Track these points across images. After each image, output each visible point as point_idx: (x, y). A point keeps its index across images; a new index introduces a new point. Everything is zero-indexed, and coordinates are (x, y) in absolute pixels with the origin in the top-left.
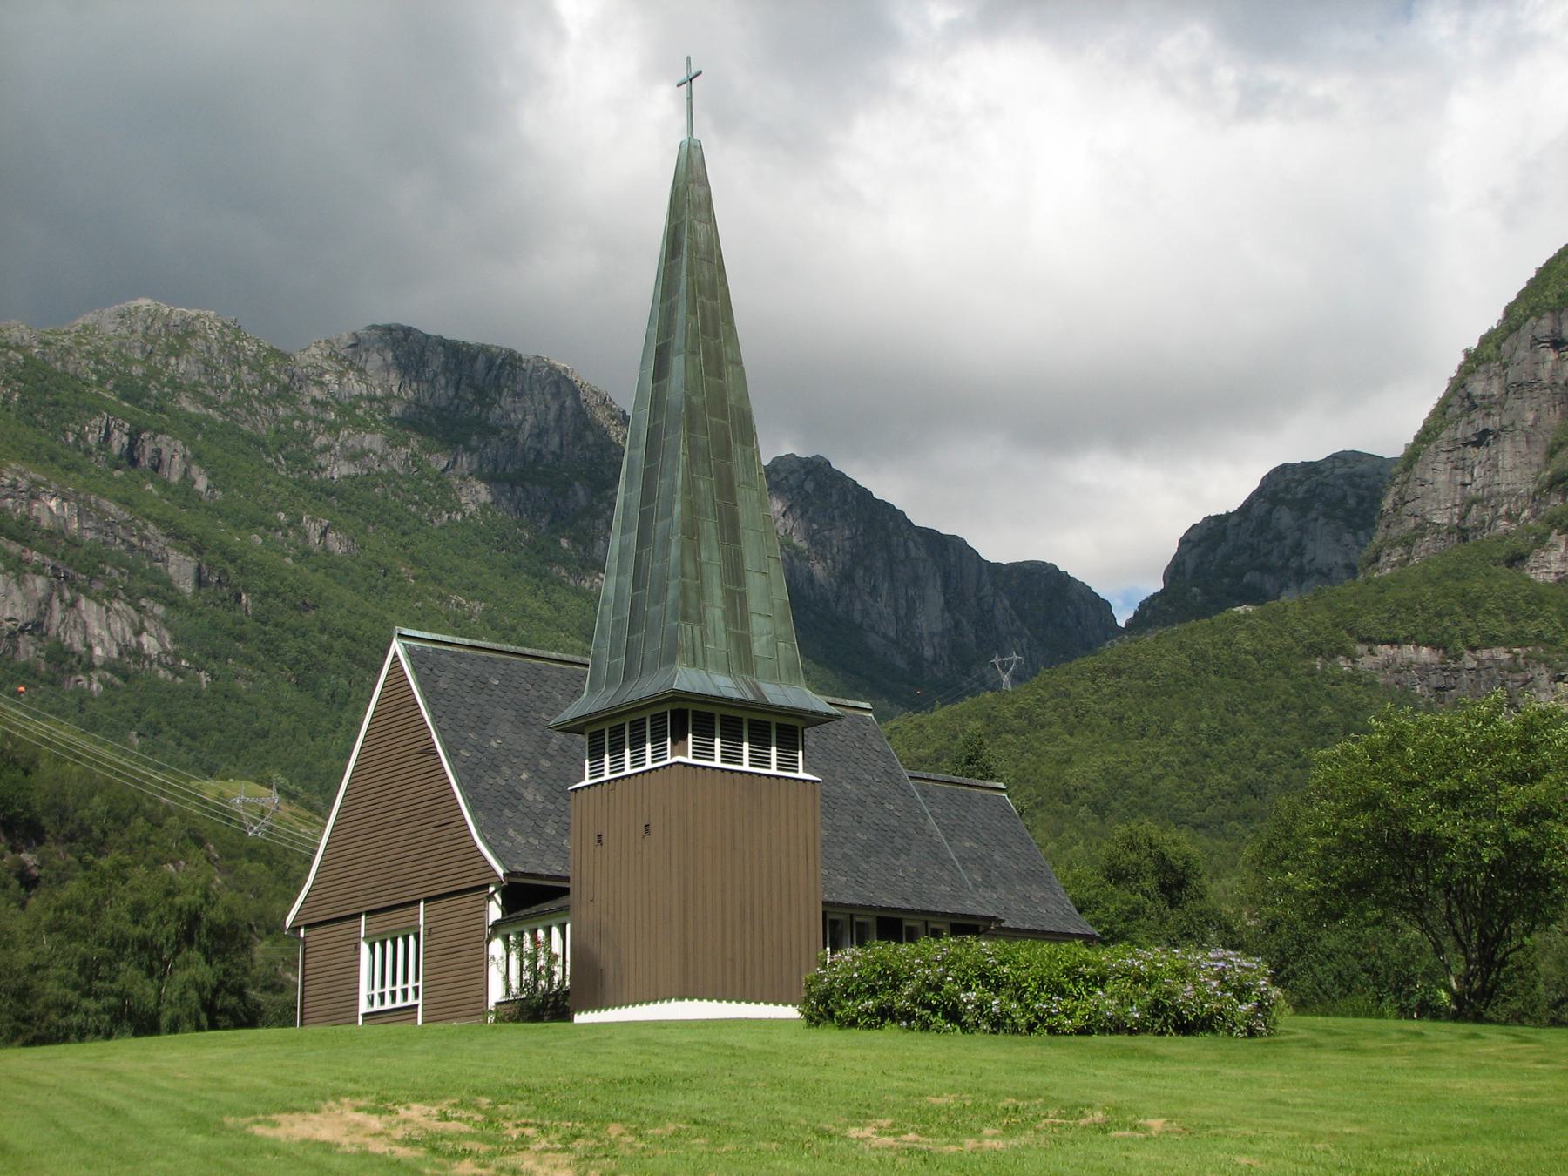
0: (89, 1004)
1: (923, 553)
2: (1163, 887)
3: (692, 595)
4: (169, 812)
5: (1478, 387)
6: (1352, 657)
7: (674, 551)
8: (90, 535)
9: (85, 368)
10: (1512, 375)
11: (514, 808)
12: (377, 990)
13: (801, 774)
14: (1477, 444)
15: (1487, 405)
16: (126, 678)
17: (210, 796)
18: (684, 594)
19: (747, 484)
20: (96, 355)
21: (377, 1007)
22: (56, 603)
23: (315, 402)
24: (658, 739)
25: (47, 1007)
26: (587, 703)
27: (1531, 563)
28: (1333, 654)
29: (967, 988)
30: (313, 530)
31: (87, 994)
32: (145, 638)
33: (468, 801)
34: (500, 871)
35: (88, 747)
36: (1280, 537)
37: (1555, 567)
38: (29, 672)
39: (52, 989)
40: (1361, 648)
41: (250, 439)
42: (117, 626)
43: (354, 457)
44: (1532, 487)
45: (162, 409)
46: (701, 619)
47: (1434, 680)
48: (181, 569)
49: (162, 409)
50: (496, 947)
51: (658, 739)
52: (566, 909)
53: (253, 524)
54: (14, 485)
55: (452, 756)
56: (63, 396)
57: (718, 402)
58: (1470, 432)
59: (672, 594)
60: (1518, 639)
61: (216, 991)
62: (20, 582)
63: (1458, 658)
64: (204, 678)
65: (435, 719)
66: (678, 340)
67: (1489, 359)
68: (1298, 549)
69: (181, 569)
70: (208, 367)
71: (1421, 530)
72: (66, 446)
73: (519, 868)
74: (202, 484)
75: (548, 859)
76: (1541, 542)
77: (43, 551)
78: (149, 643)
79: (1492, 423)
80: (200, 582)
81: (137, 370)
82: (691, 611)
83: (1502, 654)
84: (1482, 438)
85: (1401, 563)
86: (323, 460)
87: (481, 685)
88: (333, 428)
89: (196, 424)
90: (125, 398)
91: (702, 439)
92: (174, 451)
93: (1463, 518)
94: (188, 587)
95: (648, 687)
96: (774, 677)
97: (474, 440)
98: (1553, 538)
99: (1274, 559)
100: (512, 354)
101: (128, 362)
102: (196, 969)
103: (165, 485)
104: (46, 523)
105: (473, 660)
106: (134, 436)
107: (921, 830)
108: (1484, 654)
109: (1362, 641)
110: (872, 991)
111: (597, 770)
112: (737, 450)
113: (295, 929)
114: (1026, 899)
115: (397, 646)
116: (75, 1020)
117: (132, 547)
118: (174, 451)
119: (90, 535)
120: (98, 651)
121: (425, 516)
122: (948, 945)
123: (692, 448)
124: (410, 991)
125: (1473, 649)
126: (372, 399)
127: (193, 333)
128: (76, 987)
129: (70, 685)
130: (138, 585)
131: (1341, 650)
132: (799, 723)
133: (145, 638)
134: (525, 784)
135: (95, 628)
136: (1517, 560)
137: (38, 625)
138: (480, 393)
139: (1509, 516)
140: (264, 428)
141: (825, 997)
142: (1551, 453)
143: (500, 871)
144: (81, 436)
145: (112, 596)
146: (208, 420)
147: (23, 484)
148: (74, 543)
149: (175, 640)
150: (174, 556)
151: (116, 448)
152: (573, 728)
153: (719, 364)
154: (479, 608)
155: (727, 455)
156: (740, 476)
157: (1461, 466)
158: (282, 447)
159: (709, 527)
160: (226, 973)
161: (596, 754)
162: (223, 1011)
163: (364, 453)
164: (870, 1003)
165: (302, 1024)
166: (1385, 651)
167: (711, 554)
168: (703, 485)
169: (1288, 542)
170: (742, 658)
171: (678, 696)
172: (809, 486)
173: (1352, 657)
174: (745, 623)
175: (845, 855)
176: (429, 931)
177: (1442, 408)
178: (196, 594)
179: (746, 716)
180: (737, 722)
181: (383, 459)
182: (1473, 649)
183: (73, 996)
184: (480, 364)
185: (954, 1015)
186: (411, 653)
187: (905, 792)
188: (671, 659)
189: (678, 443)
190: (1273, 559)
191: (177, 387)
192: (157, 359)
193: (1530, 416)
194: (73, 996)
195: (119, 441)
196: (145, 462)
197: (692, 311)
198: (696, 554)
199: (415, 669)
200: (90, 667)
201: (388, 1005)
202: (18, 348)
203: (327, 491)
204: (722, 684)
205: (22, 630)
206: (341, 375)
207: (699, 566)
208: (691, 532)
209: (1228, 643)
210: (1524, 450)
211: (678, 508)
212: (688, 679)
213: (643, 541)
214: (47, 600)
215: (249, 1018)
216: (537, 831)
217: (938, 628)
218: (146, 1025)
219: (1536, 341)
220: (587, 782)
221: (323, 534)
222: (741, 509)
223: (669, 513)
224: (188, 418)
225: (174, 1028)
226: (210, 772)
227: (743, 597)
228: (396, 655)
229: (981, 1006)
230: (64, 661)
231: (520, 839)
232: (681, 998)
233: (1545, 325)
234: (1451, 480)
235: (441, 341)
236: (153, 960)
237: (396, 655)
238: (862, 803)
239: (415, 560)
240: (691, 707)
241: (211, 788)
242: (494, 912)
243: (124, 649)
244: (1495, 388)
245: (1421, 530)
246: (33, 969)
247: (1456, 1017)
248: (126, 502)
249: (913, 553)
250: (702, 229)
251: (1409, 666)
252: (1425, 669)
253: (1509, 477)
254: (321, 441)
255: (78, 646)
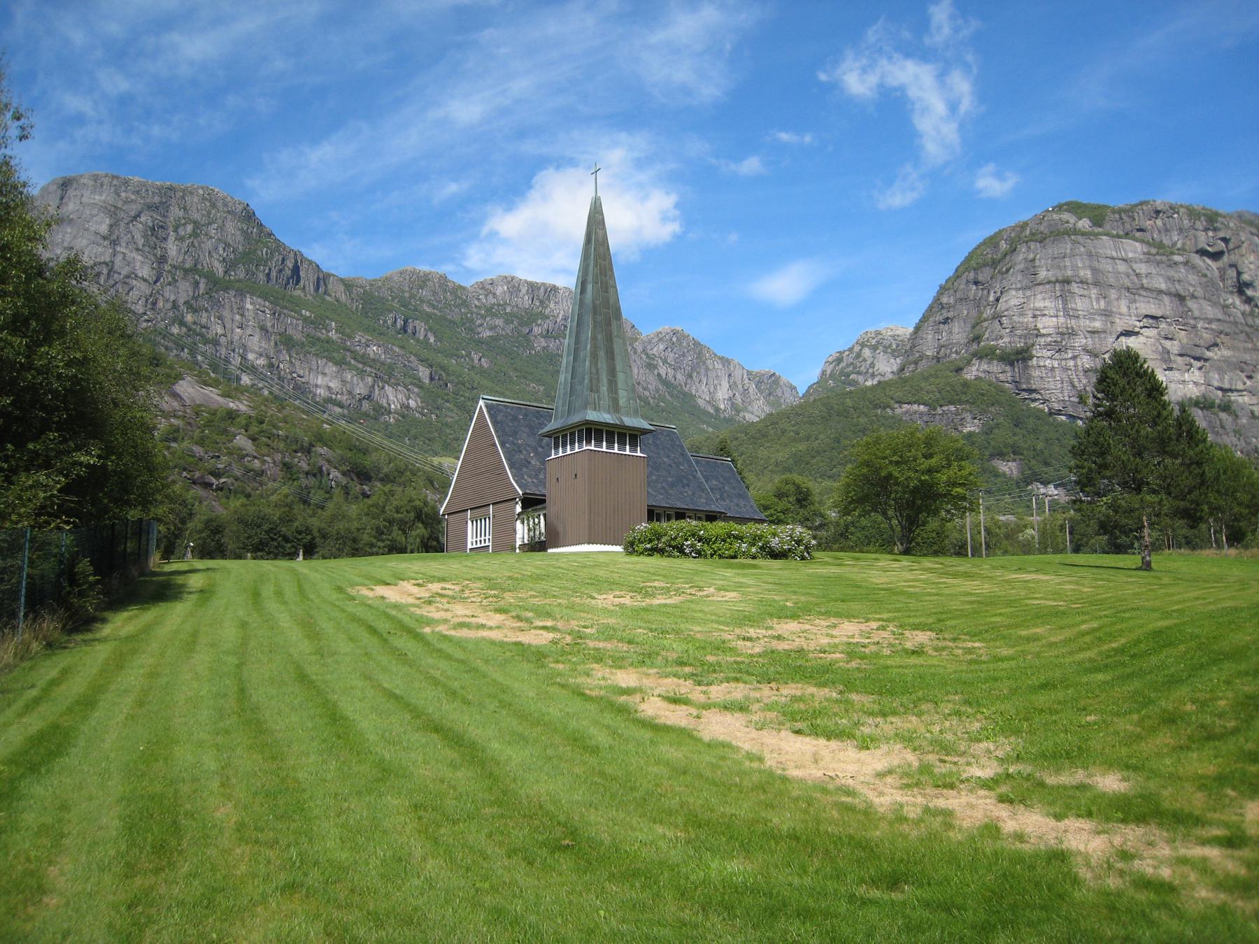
0: (381, 544)
1: (720, 366)
2: (798, 501)
3: (594, 382)
4: (419, 470)
5: (945, 300)
6: (893, 409)
7: (587, 363)
8: (389, 360)
9: (386, 294)
10: (959, 295)
11: (527, 467)
12: (483, 538)
13: (639, 454)
14: (944, 323)
15: (949, 307)
16: (403, 417)
17: (436, 463)
18: (591, 381)
19: (617, 336)
20: (391, 289)
21: (474, 546)
22: (376, 387)
23: (476, 306)
24: (580, 441)
25: (365, 545)
26: (552, 425)
27: (965, 371)
28: (884, 408)
29: (687, 540)
30: (476, 357)
31: (378, 540)
32: (410, 401)
33: (508, 464)
34: (521, 493)
35: (388, 444)
36: (865, 360)
37: (974, 373)
38: (366, 415)
39: (366, 538)
40: (897, 405)
41: (451, 321)
42: (400, 396)
43: (492, 328)
44: (966, 341)
45: (416, 310)
46: (598, 391)
47: (925, 418)
48: (424, 373)
49: (416, 310)
50: (518, 524)
51: (580, 441)
52: (544, 508)
53: (452, 356)
54: (360, 341)
55: (503, 445)
56: (379, 306)
57: (606, 303)
58: (941, 318)
59: (586, 381)
60: (960, 402)
61: (428, 539)
62: (362, 379)
63: (935, 409)
64: (433, 416)
65: (496, 432)
66: (590, 278)
67: (949, 289)
68: (872, 365)
69: (424, 373)
70: (434, 293)
71: (921, 357)
72: (379, 325)
73: (528, 491)
74: (432, 340)
75: (540, 488)
76: (969, 363)
77: (371, 367)
78: (412, 403)
79: (950, 315)
80: (432, 379)
81: (407, 295)
82: (594, 388)
83: (952, 408)
84: (946, 321)
85: (913, 371)
86: (480, 330)
87: (515, 419)
88: (483, 317)
89: (429, 316)
90: (403, 306)
91: (599, 318)
92: (421, 327)
93: (938, 353)
94: (427, 381)
95: (576, 418)
96: (627, 415)
97: (539, 321)
98: (974, 361)
99: (863, 369)
100: (554, 286)
101: (403, 292)
102: (420, 530)
103: (418, 340)
104: (372, 356)
105: (513, 408)
106: (406, 322)
107: (694, 477)
108: (945, 408)
109: (897, 402)
110: (650, 541)
111: (556, 453)
112: (614, 323)
113: (444, 515)
114: (738, 505)
115: (481, 403)
116: (374, 550)
117: (405, 366)
118: (421, 327)
119: (389, 360)
120: (393, 406)
121: (520, 352)
122: (675, 524)
123: (595, 322)
124: (487, 540)
125: (941, 406)
126: (499, 305)
127: (429, 280)
128: (375, 537)
129: (382, 419)
130: (408, 380)
131: (889, 406)
132: (639, 434)
133: (410, 401)
134: (532, 458)
135: (391, 398)
136: (959, 370)
137: (369, 396)
138: (542, 302)
139: (956, 352)
140: (457, 318)
141: (632, 544)
142: (973, 327)
143: (521, 493)
144: (385, 322)
145: (398, 384)
146: (434, 314)
147: (363, 341)
148: (383, 364)
149: (422, 402)
150: (421, 368)
151: (398, 326)
152: (549, 435)
153: (607, 288)
154: (542, 388)
155: (609, 324)
156: (615, 333)
157: (938, 332)
158: (464, 325)
159: (602, 354)
160: (432, 532)
161: (556, 448)
162: (431, 547)
163: (496, 327)
164: (648, 546)
165: (973, 555)
166: (906, 406)
167: (603, 365)
168: (599, 337)
169: (868, 362)
170: (615, 408)
171: (588, 422)
172: (674, 339)
173: (893, 409)
174: (616, 393)
175: (663, 488)
176: (494, 516)
177: (930, 308)
178: (430, 384)
179: (628, 432)
180: (613, 433)
181: (503, 329)
182: (941, 406)
183: (374, 541)
184: (542, 290)
185: (681, 551)
186: (487, 406)
187: (689, 461)
188: (586, 408)
189: (589, 320)
190: (862, 368)
191: (422, 301)
192: (414, 291)
193: (965, 312)
194: (374, 541)
195: (400, 323)
196: (409, 331)
197: (596, 265)
198: (596, 364)
199: (489, 412)
200: (390, 412)
201: (479, 545)
202: (361, 287)
203: (481, 342)
204: (607, 418)
205: (364, 398)
206: (486, 296)
207: (597, 370)
208: (594, 356)
209: (843, 403)
210: (962, 325)
211: (589, 346)
212: (592, 415)
213: (575, 360)
214: (373, 386)
215: (439, 548)
216: (536, 476)
217: (726, 397)
218: (402, 550)
219: (968, 282)
220: (553, 457)
221: (480, 360)
222: (615, 347)
223: (586, 348)
224: (427, 314)
225: (412, 552)
226: (436, 454)
227: (616, 382)
228: (481, 407)
229: (692, 546)
230: (380, 410)
231: (530, 480)
232: (589, 543)
233: (972, 275)
234: (933, 338)
235: (526, 282)
236: (404, 527)
237: (481, 407)
238: (670, 466)
239: (516, 369)
240: (593, 427)
241: (436, 460)
242: (519, 509)
243: (402, 405)
244: (952, 301)
245: (921, 357)
246: (358, 530)
247: (1043, 550)
248: (402, 347)
249: (716, 366)
250: (600, 232)
251: (915, 413)
252: (922, 414)
253: (957, 337)
254: (479, 322)
255: (385, 404)
